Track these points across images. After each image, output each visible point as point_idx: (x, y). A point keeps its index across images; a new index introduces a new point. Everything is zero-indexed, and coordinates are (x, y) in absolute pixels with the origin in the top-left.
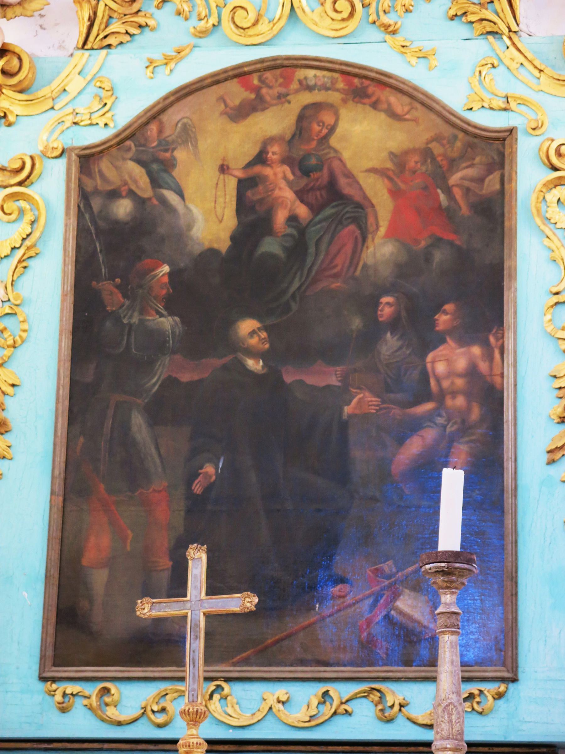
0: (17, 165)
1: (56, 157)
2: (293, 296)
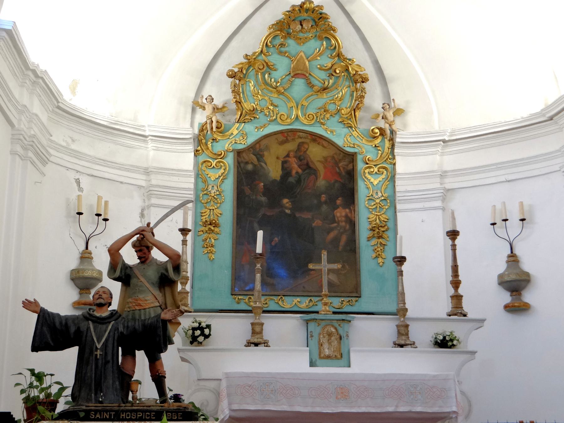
0: (220, 153)
1: (231, 152)
2: (298, 194)
